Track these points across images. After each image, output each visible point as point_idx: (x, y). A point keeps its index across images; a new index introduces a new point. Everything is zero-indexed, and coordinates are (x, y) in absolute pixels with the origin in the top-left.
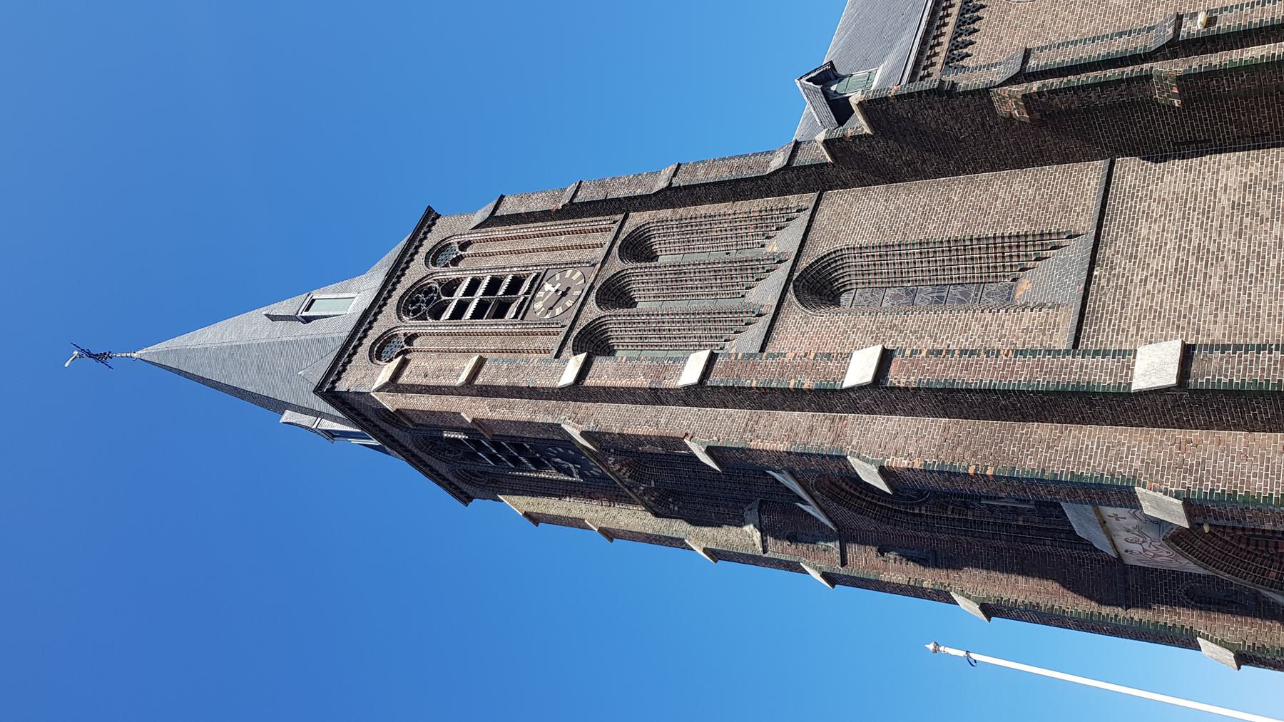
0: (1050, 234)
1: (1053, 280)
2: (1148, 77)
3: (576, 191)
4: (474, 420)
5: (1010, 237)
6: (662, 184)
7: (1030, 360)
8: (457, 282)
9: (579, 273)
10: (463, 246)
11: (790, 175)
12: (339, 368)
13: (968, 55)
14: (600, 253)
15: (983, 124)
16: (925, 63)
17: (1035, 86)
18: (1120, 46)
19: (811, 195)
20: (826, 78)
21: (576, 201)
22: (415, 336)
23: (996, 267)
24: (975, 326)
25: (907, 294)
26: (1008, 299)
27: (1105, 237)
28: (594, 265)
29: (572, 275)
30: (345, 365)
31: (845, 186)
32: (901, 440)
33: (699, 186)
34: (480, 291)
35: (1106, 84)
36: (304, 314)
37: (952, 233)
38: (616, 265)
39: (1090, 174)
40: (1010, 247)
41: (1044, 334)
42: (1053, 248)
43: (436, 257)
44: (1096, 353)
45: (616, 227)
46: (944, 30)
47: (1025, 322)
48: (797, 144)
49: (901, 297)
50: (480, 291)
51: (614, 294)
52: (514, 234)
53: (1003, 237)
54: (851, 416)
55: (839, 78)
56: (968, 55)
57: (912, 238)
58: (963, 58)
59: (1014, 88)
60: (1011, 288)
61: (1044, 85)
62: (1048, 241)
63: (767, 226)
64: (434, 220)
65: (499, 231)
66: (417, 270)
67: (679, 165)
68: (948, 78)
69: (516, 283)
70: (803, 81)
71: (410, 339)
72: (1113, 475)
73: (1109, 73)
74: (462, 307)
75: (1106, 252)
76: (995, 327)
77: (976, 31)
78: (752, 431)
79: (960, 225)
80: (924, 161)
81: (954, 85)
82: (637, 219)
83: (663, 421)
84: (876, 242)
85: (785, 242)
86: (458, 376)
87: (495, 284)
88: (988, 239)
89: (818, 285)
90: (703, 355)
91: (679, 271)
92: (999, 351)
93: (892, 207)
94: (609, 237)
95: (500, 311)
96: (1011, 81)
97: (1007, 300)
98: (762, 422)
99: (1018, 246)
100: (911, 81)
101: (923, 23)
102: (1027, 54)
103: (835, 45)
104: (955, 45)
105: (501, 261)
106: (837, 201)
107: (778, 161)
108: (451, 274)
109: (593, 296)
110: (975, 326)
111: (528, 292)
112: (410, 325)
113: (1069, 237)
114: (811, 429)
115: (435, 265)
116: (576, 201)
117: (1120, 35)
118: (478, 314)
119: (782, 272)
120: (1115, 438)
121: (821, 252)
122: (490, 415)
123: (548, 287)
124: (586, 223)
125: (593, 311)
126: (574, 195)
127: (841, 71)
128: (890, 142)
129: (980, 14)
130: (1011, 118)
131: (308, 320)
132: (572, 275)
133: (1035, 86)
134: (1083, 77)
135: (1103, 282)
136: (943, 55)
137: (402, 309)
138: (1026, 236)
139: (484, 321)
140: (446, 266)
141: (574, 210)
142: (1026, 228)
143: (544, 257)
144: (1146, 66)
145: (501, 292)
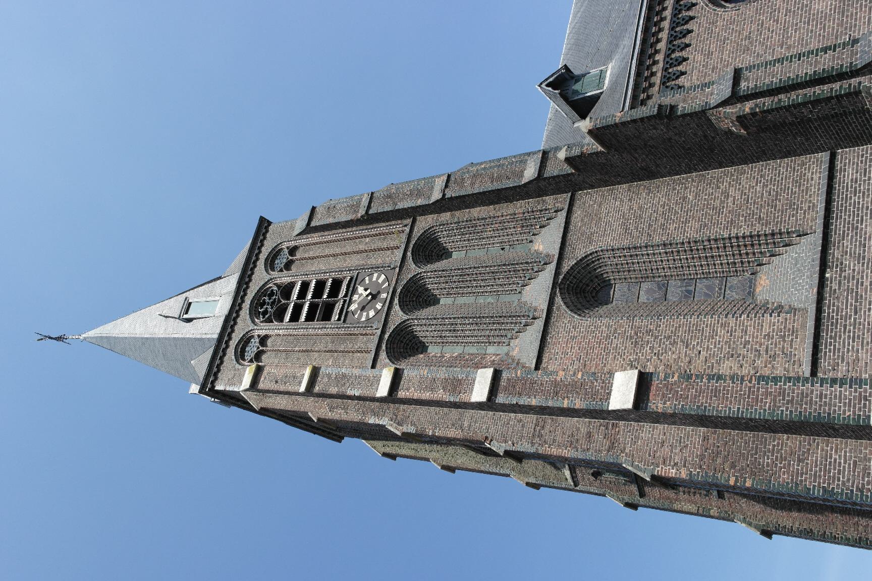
0: (781, 234)
1: (787, 279)
2: (857, 93)
3: (370, 203)
4: (319, 419)
5: (744, 237)
6: (436, 196)
7: (772, 388)
8: (292, 285)
9: (383, 277)
10: (293, 251)
11: (542, 184)
12: (221, 354)
13: (683, 73)
14: (399, 254)
15: (705, 136)
16: (652, 40)
17: (748, 107)
18: (826, 63)
19: (564, 195)
20: (562, 83)
21: (371, 212)
22: (266, 337)
23: (735, 263)
24: (721, 332)
25: (660, 288)
26: (749, 293)
27: (834, 238)
28: (394, 268)
29: (378, 278)
30: (218, 367)
31: (592, 187)
32: (666, 449)
33: (468, 195)
34: (309, 296)
35: (817, 102)
36: (185, 316)
37: (692, 232)
38: (412, 269)
39: (814, 167)
40: (745, 246)
41: (784, 341)
42: (786, 245)
43: (273, 262)
44: (834, 381)
45: (407, 229)
46: (653, 80)
47: (766, 329)
48: (545, 154)
49: (655, 292)
50: (309, 296)
51: (415, 296)
52: (329, 238)
53: (737, 238)
54: (622, 423)
55: (577, 79)
56: (683, 73)
57: (657, 240)
58: (678, 77)
59: (729, 110)
60: (751, 281)
61: (756, 105)
62: (779, 240)
63: (531, 225)
64: (267, 229)
65: (315, 238)
66: (260, 276)
67: (449, 176)
68: (667, 100)
69: (337, 284)
70: (543, 86)
71: (263, 340)
72: (862, 492)
73: (817, 90)
74: (298, 309)
75: (835, 253)
76: (738, 333)
77: (688, 46)
78: (540, 436)
79: (697, 225)
80: (657, 166)
81: (673, 108)
82: (424, 223)
83: (466, 424)
84: (626, 243)
85: (547, 242)
86: (300, 382)
87: (320, 285)
88: (723, 239)
89: (583, 287)
90: (489, 373)
91: (463, 273)
92: (743, 377)
93: (635, 207)
94: (404, 237)
95: (327, 317)
96: (724, 103)
97: (748, 304)
98: (548, 427)
99: (752, 245)
100: (632, 107)
101: (638, 42)
102: (737, 75)
103: (575, 16)
104: (671, 62)
105: (322, 265)
106: (588, 199)
107: (530, 172)
108: (285, 278)
109: (396, 308)
110: (721, 332)
111: (346, 296)
112: (262, 329)
113: (799, 236)
114: (589, 435)
115: (273, 270)
116: (371, 212)
117: (825, 50)
118: (310, 318)
119: (545, 278)
120: (861, 452)
121: (580, 254)
122: (330, 415)
123: (360, 290)
124: (382, 227)
125: (398, 316)
126: (369, 207)
127: (576, 72)
128: (624, 155)
129: (688, 27)
130: (729, 132)
131: (189, 320)
132: (378, 278)
133: (748, 107)
134: (793, 95)
135: (835, 286)
136: (659, 75)
137: (254, 313)
138: (759, 236)
139: (315, 322)
140: (281, 271)
141: (370, 219)
142: (758, 228)
143: (355, 261)
144: (854, 81)
145: (325, 297)
